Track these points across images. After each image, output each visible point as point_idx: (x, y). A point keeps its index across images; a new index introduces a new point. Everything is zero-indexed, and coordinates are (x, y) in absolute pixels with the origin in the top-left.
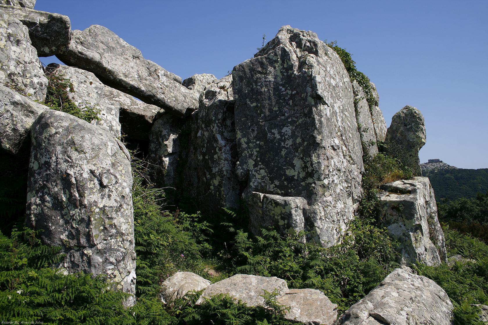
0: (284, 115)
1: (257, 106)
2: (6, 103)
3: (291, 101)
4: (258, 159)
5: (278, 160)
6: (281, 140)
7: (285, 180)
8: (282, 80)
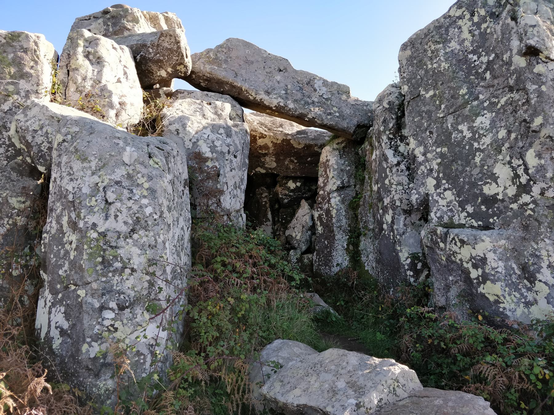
0: (477, 98)
1: (435, 95)
2: (40, 118)
3: (488, 72)
4: (441, 175)
5: (470, 171)
6: (473, 139)
7: (482, 203)
8: (472, 43)
